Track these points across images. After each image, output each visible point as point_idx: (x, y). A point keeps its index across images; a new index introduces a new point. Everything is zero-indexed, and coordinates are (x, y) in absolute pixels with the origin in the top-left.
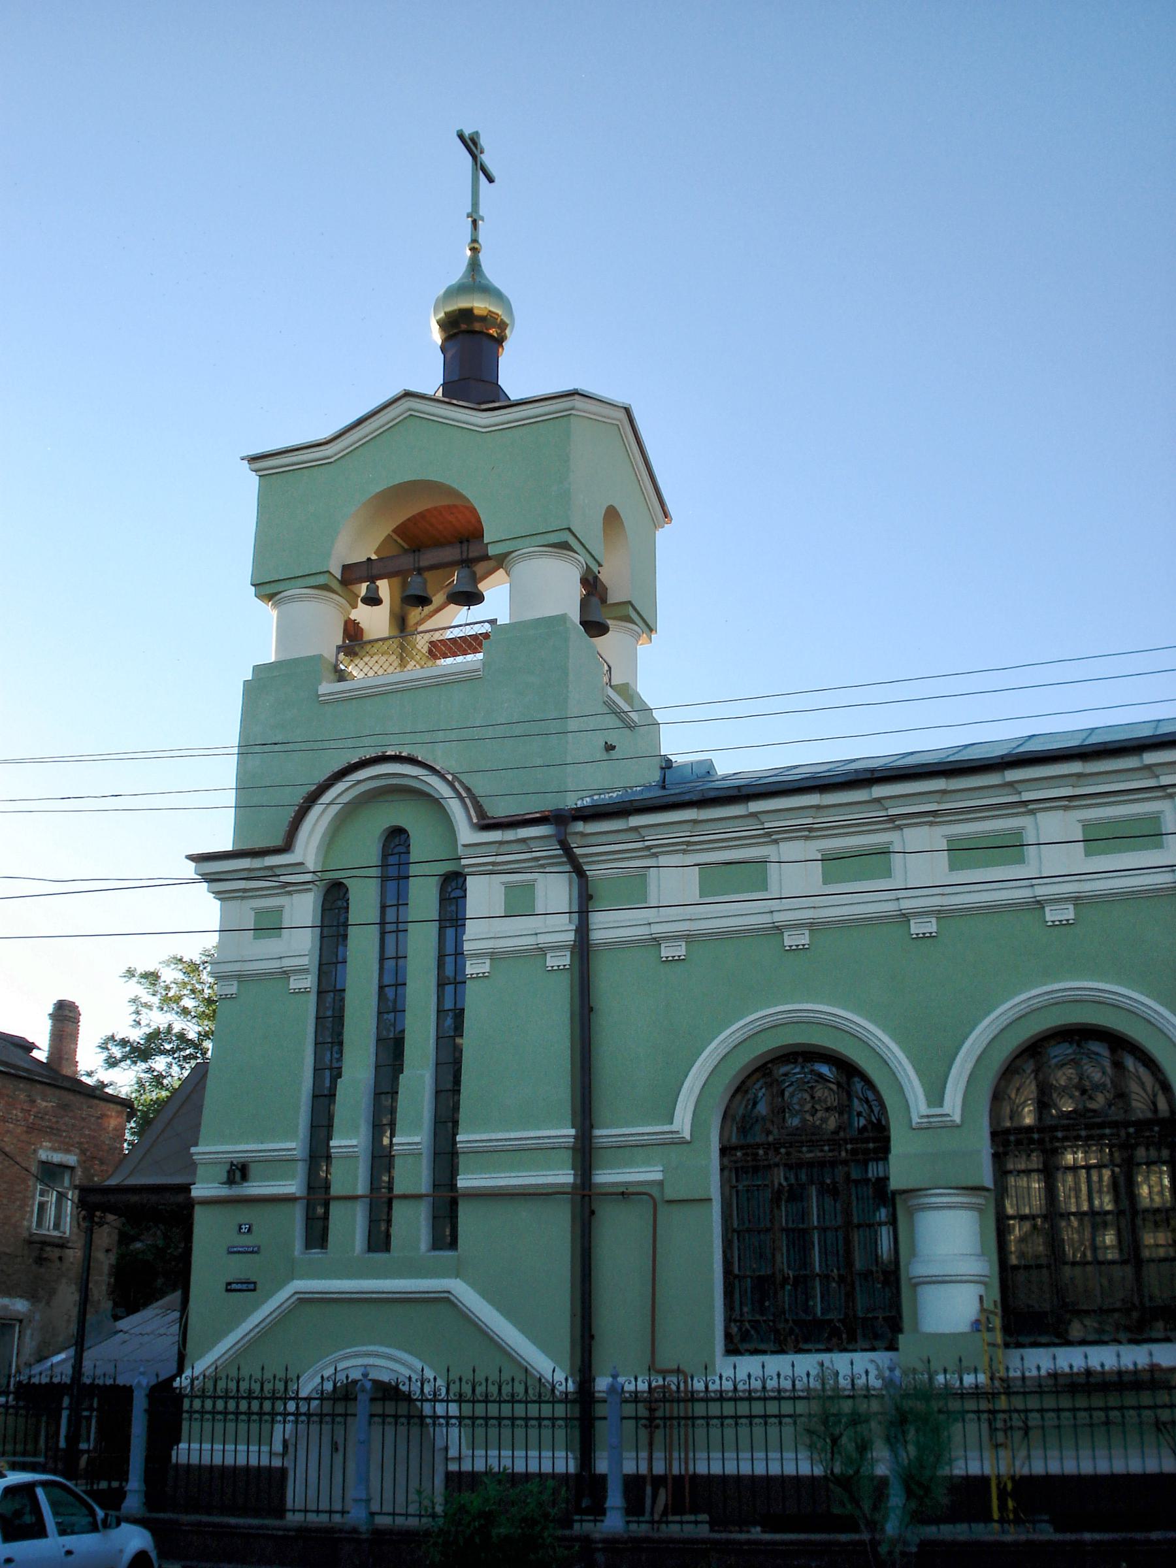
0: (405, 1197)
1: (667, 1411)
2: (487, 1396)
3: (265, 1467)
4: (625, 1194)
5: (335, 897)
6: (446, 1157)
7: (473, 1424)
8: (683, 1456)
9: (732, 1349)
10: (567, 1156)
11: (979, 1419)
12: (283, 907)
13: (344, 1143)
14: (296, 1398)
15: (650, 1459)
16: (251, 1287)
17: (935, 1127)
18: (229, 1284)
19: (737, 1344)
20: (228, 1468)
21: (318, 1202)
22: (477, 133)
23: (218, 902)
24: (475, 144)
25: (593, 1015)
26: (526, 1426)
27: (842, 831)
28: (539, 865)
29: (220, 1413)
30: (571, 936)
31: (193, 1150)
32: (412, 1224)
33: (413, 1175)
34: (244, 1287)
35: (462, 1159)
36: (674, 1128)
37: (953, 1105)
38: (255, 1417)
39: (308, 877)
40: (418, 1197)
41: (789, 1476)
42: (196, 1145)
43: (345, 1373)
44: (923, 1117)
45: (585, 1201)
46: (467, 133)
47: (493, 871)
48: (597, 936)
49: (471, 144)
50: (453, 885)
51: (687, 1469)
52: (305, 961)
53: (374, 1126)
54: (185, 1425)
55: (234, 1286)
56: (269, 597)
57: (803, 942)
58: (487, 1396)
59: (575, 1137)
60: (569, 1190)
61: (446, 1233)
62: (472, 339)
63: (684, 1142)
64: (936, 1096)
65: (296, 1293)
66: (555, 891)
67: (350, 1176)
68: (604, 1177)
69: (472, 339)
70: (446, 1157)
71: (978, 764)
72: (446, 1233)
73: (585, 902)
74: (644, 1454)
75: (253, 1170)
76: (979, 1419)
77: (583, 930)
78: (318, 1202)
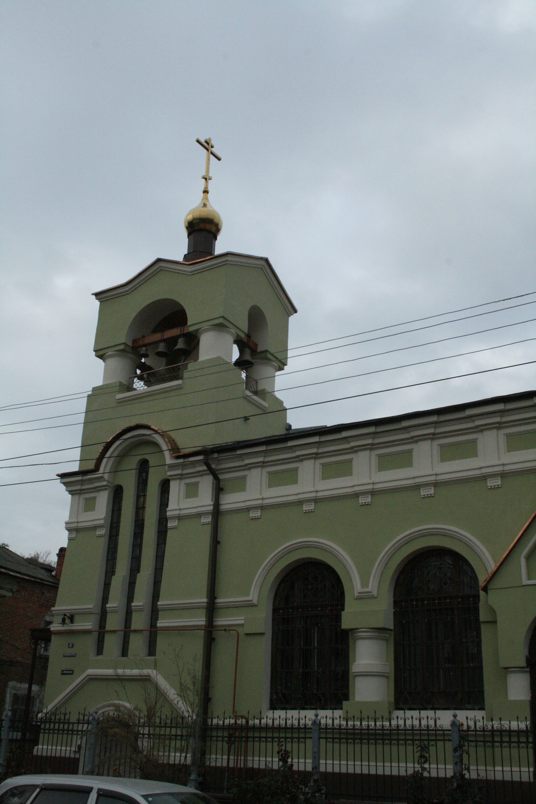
0: (135, 631)
1: (241, 735)
2: (413, 727)
3: (39, 756)
4: (227, 629)
5: (117, 493)
6: (154, 613)
7: (273, 740)
8: (236, 758)
9: (273, 707)
10: (204, 612)
11: (527, 747)
12: (413, 449)
13: (166, 603)
14: (69, 723)
15: (228, 759)
16: (71, 672)
17: (364, 597)
18: (63, 671)
19: (277, 702)
20: (57, 757)
21: (102, 632)
22: (210, 139)
23: (70, 496)
24: (208, 144)
25: (218, 546)
26: (391, 744)
27: (445, 435)
28: (200, 474)
29: (61, 730)
30: (211, 508)
31: (53, 609)
32: (138, 644)
33: (139, 621)
34: (69, 672)
35: (160, 613)
36: (250, 598)
37: (372, 587)
38: (61, 732)
39: (105, 483)
40: (141, 631)
41: (365, 774)
42: (54, 606)
43: (107, 713)
44: (359, 593)
45: (210, 634)
46: (203, 141)
47: (181, 477)
48: (223, 507)
49: (207, 145)
50: (165, 486)
51: (237, 765)
52: (102, 522)
53: (128, 598)
54: (41, 735)
55: (65, 672)
56: (101, 357)
57: (257, 515)
58: (413, 727)
59: (207, 603)
60: (203, 628)
61: (152, 651)
62: (202, 230)
63: (373, 597)
64: (365, 582)
65: (88, 675)
66: (206, 485)
67: (114, 622)
68: (221, 621)
69: (202, 230)
70: (154, 613)
71: (250, 443)
72: (152, 651)
73: (219, 490)
74: (225, 757)
75: (76, 618)
76: (527, 747)
77: (217, 504)
78: (102, 632)
